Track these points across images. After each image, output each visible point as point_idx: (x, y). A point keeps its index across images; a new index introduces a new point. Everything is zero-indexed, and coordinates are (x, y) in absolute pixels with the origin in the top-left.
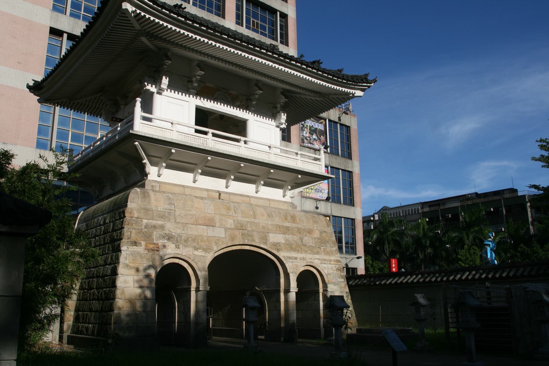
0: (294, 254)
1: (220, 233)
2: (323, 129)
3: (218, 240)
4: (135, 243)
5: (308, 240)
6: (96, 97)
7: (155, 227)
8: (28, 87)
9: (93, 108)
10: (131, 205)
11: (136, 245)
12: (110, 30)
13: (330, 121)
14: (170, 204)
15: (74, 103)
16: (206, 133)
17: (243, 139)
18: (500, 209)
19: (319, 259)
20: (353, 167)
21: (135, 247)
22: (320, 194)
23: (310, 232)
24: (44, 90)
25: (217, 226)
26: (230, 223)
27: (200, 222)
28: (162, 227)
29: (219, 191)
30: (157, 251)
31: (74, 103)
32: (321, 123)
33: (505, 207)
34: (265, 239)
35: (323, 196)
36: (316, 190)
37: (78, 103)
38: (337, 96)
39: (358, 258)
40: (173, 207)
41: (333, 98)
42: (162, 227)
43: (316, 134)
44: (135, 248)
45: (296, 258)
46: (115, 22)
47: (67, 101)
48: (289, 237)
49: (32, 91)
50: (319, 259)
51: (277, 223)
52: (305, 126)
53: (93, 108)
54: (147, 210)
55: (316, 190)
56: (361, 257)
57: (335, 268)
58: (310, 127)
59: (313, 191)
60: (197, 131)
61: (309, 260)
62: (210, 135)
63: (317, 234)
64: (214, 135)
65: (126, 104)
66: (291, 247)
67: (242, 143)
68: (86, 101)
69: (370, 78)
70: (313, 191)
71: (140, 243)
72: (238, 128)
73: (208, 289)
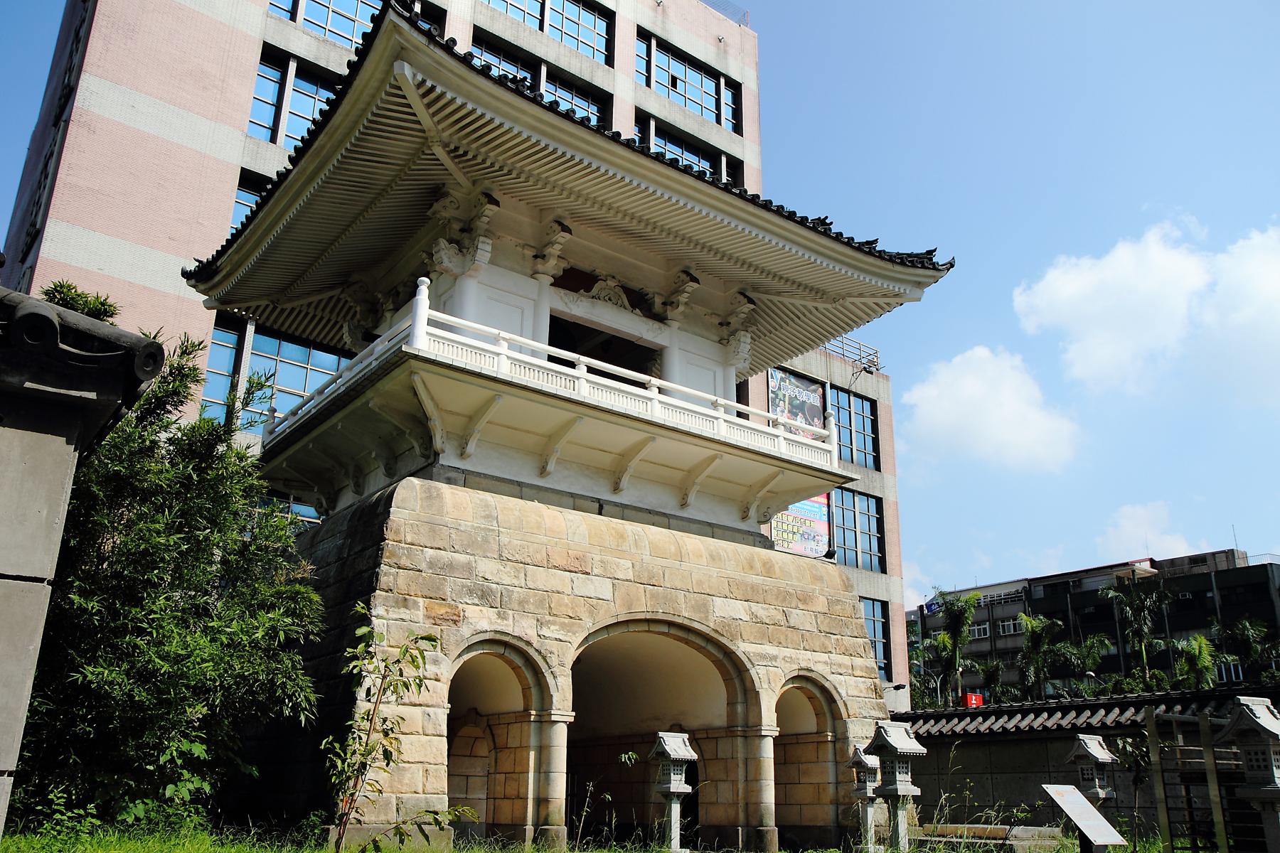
0: (770, 649)
1: (602, 588)
2: (818, 403)
3: (593, 603)
4: (405, 603)
5: (799, 617)
6: (331, 298)
7: (451, 566)
8: (186, 274)
9: (324, 322)
10: (399, 515)
11: (406, 607)
12: (366, 128)
13: (833, 386)
14: (487, 517)
15: (283, 311)
16: (572, 365)
17: (655, 381)
18: (1210, 595)
19: (826, 663)
20: (883, 487)
21: (403, 610)
22: (812, 544)
23: (805, 599)
24: (217, 278)
25: (596, 571)
26: (624, 569)
27: (557, 560)
28: (469, 568)
29: (598, 500)
30: (455, 622)
31: (283, 311)
32: (814, 391)
33: (1219, 589)
34: (704, 608)
35: (820, 549)
36: (802, 535)
37: (293, 310)
38: (863, 300)
39: (897, 688)
40: (495, 523)
41: (853, 303)
42: (469, 568)
43: (804, 414)
44: (404, 613)
45: (775, 658)
46: (378, 108)
47: (267, 306)
48: (760, 610)
49: (193, 282)
50: (826, 663)
51: (730, 573)
52: (781, 396)
53: (324, 322)
54: (433, 527)
55: (802, 535)
56: (903, 687)
57: (862, 686)
58: (790, 398)
59: (797, 537)
60: (552, 359)
61: (803, 665)
62: (581, 371)
63: (821, 604)
64: (591, 370)
65: (396, 309)
66: (765, 630)
67: (653, 393)
68: (309, 305)
69: (939, 258)
70: (797, 537)
71: (416, 603)
72: (642, 359)
73: (572, 720)
